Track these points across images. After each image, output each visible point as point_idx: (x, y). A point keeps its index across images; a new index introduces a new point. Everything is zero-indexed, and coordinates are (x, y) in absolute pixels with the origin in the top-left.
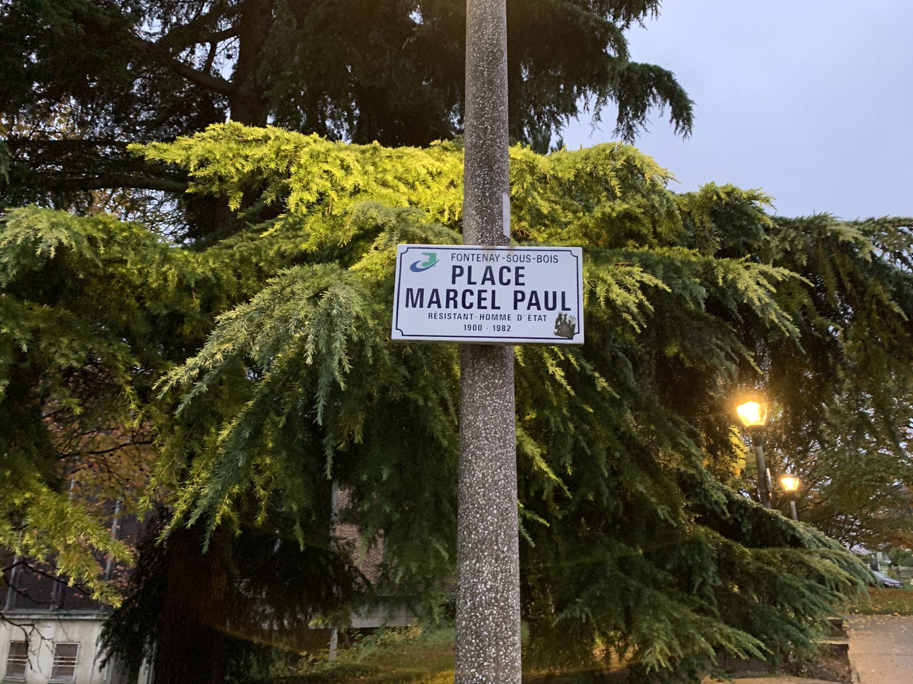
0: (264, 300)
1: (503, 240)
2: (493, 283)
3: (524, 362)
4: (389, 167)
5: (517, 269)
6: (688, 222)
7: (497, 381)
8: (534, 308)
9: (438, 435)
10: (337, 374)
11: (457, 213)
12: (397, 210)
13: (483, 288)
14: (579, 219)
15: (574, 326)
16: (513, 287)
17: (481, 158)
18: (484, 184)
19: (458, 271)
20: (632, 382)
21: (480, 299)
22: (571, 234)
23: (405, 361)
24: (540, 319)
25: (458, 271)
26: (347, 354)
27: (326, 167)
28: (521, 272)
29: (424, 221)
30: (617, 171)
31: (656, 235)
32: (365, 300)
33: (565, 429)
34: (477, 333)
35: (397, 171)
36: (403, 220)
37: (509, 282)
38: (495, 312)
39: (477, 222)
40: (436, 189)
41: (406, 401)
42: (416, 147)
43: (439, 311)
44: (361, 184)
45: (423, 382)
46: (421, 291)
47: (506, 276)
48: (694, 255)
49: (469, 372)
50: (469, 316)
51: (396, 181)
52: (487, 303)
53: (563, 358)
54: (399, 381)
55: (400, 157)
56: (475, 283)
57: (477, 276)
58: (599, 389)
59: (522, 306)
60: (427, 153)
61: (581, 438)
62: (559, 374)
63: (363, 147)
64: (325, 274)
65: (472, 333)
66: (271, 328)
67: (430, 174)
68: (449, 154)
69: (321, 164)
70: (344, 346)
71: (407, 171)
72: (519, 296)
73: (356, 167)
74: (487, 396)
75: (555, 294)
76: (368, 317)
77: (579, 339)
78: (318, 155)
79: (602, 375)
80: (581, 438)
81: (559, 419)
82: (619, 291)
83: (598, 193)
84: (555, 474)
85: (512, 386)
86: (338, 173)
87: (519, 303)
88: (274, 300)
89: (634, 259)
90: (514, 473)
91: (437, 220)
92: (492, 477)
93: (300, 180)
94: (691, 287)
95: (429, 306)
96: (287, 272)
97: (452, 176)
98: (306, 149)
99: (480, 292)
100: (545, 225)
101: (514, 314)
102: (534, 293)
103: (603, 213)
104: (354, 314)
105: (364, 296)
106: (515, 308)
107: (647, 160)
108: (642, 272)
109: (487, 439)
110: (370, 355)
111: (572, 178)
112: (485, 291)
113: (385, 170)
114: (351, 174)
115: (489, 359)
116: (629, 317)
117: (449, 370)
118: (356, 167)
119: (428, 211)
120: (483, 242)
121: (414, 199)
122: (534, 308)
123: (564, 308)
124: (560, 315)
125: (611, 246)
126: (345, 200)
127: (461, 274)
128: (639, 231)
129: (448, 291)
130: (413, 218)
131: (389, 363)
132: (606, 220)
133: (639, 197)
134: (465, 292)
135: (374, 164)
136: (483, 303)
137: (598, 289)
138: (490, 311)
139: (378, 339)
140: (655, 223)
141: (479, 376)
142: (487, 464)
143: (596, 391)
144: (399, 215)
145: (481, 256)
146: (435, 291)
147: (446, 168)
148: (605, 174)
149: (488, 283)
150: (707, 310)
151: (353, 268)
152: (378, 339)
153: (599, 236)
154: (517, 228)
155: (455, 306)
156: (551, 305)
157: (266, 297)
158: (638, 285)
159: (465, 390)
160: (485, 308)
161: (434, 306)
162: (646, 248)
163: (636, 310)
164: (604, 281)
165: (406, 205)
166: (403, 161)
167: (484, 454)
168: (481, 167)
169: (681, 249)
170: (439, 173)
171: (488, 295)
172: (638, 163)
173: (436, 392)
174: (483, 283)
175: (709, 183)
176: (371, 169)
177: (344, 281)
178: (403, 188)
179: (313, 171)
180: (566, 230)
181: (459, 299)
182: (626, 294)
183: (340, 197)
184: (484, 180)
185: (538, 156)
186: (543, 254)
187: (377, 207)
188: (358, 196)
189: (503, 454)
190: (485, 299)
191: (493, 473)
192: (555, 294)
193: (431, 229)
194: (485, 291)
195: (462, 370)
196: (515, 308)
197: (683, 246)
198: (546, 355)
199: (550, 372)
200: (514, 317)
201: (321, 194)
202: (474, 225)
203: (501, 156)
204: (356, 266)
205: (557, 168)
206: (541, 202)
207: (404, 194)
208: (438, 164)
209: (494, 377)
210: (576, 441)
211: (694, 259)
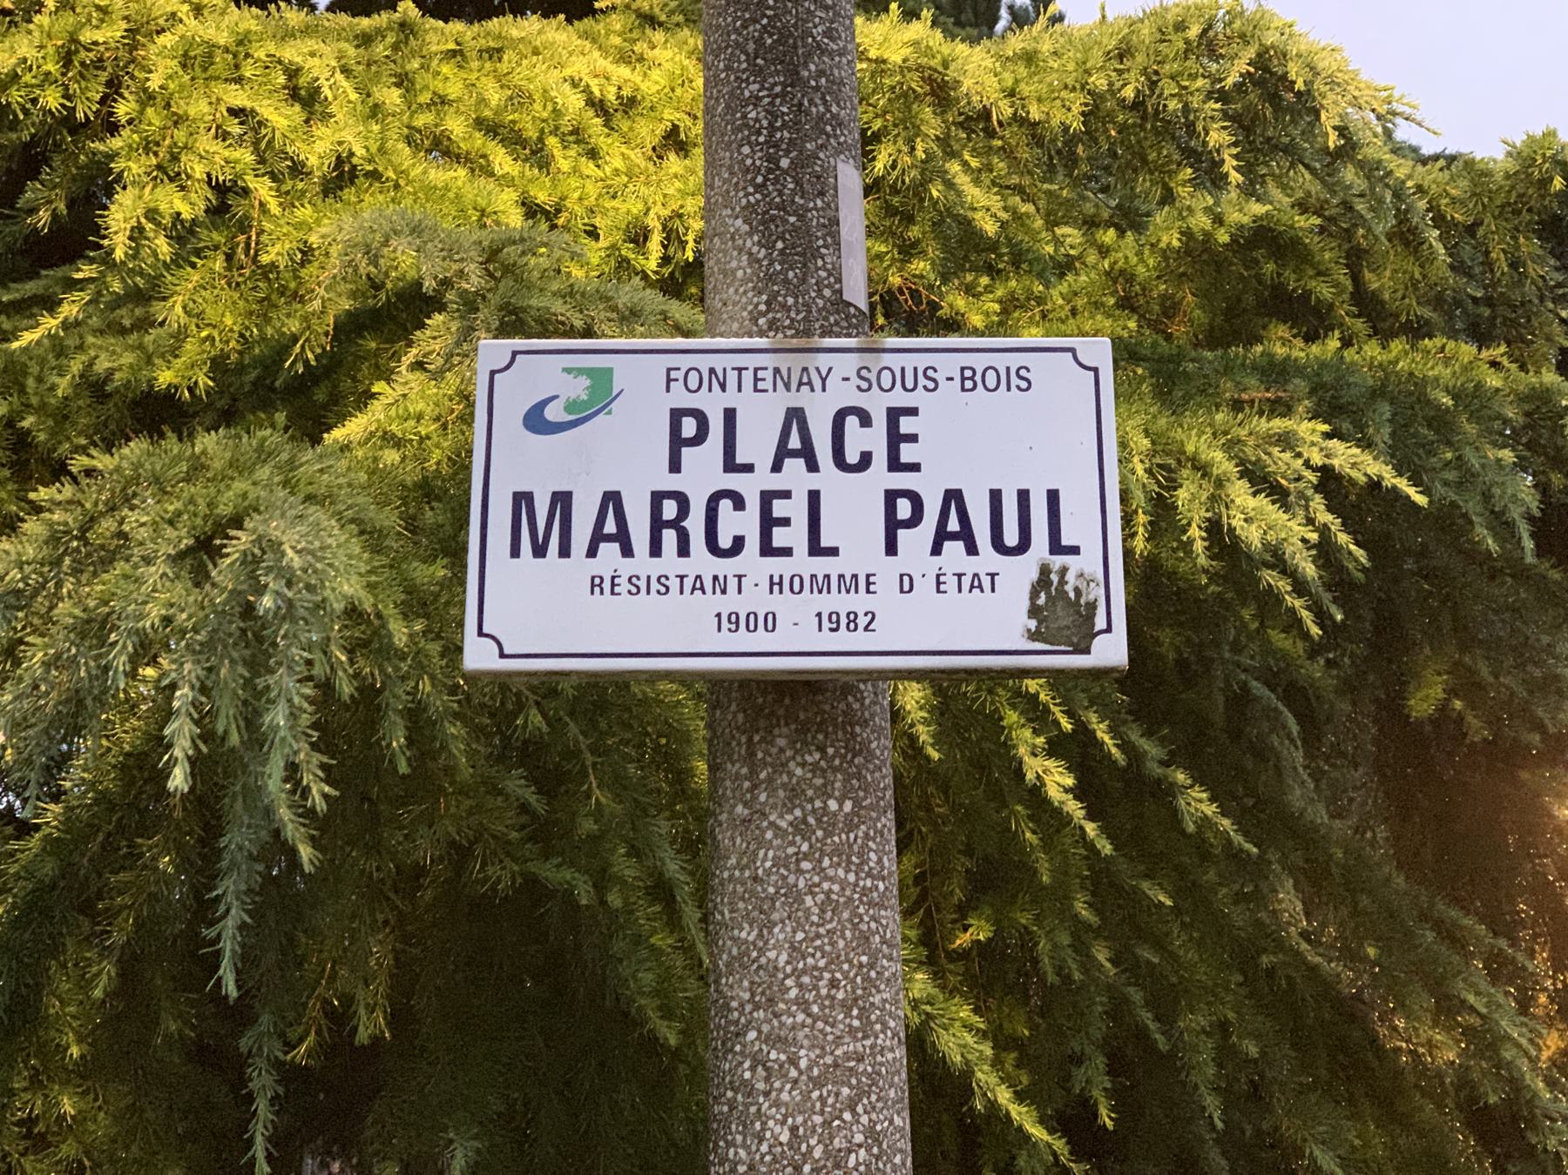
0: (20, 565)
1: (840, 316)
2: (813, 466)
3: (938, 741)
4: (454, 90)
5: (894, 415)
6: (1467, 251)
7: (833, 805)
8: (954, 548)
9: (649, 1007)
10: (284, 813)
11: (690, 238)
12: (486, 237)
13: (776, 482)
14: (1104, 251)
15: (1092, 606)
16: (880, 477)
17: (759, 42)
18: (772, 129)
19: (689, 427)
20: (1301, 795)
21: (768, 522)
22: (1080, 302)
23: (530, 754)
24: (976, 585)
25: (689, 427)
26: (314, 746)
27: (238, 97)
28: (906, 425)
29: (578, 273)
30: (1223, 96)
31: (1365, 303)
32: (377, 550)
33: (1085, 971)
34: (761, 640)
35: (482, 101)
36: (508, 269)
37: (866, 460)
38: (821, 565)
39: (753, 259)
40: (618, 163)
41: (532, 887)
42: (545, 16)
43: (626, 567)
44: (359, 151)
45: (588, 826)
46: (562, 500)
47: (857, 440)
48: (1494, 364)
49: (737, 776)
50: (732, 584)
51: (479, 139)
52: (793, 536)
53: (1066, 725)
54: (506, 825)
55: (494, 54)
56: (749, 468)
57: (757, 444)
58: (1191, 828)
59: (914, 542)
60: (585, 35)
61: (1136, 995)
62: (1057, 780)
63: (365, 23)
64: (238, 467)
65: (744, 640)
66: (47, 665)
67: (597, 105)
68: (658, 36)
69: (218, 89)
70: (305, 720)
71: (520, 99)
72: (904, 509)
73: (340, 92)
74: (800, 857)
75: (1023, 496)
76: (390, 611)
77: (1111, 650)
78: (210, 55)
79: (1200, 779)
80: (1136, 995)
81: (1065, 939)
82: (1252, 503)
83: (1163, 172)
84: (1042, 1121)
85: (888, 821)
86: (280, 117)
87: (901, 533)
88: (57, 562)
89: (1300, 385)
90: (902, 1121)
91: (623, 265)
92: (826, 1142)
93: (148, 146)
94: (1490, 476)
95: (592, 552)
96: (102, 461)
97: (670, 115)
98: (166, 40)
99: (767, 498)
100: (992, 270)
101: (887, 570)
102: (953, 497)
103: (1187, 234)
104: (339, 606)
105: (372, 538)
106: (891, 548)
107: (1324, 63)
108: (1328, 436)
109: (804, 1005)
110: (398, 741)
111: (1076, 125)
112: (786, 495)
113: (441, 101)
114: (326, 117)
115: (803, 730)
116: (1284, 585)
117: (681, 776)
118: (340, 92)
119: (593, 234)
120: (773, 326)
121: (542, 197)
122: (954, 548)
123: (1056, 547)
124: (1045, 571)
125: (1215, 338)
126: (305, 213)
127: (699, 438)
128: (1307, 294)
129: (658, 498)
130: (544, 262)
131: (465, 772)
132: (1196, 250)
133: (1304, 180)
134: (715, 499)
135: (403, 81)
136: (780, 537)
137: (1182, 495)
138: (803, 563)
139: (426, 686)
140: (1356, 258)
141: (772, 792)
142: (806, 1096)
143: (1183, 832)
144: (492, 254)
145: (768, 375)
146: (612, 499)
147: (651, 84)
148: (1186, 109)
149: (794, 466)
150: (1540, 552)
151: (338, 434)
152: (426, 686)
153: (1170, 308)
154: (895, 280)
155: (684, 550)
156: (1011, 537)
157: (30, 552)
158: (1312, 477)
159: (724, 838)
160: (787, 552)
161: (609, 550)
162: (1333, 343)
163: (1310, 570)
164: (1203, 469)
165: (515, 219)
166: (503, 67)
167: (793, 1062)
168: (759, 72)
169: (1451, 345)
170: (629, 104)
171: (794, 509)
172: (1297, 74)
173: (634, 852)
174: (777, 467)
175: (1538, 133)
176: (392, 97)
177: (304, 490)
178: (502, 160)
179: (192, 112)
180: (1064, 287)
181: (695, 524)
182: (1275, 514)
183: (289, 200)
184: (772, 114)
185: (961, 49)
186: (979, 362)
187: (416, 230)
188: (349, 194)
189: (860, 1059)
190: (785, 522)
191: (827, 1124)
192: (1023, 496)
193: (606, 298)
194: (786, 495)
195: (713, 768)
196: (891, 548)
197: (1453, 334)
198: (1012, 717)
199: (1030, 776)
200: (886, 582)
201: (221, 189)
202: (740, 266)
203: (828, 33)
204: (352, 429)
205: (1024, 89)
206: (973, 193)
207: (506, 181)
208: (624, 72)
209: (825, 793)
210: (1118, 1009)
211: (1493, 381)
